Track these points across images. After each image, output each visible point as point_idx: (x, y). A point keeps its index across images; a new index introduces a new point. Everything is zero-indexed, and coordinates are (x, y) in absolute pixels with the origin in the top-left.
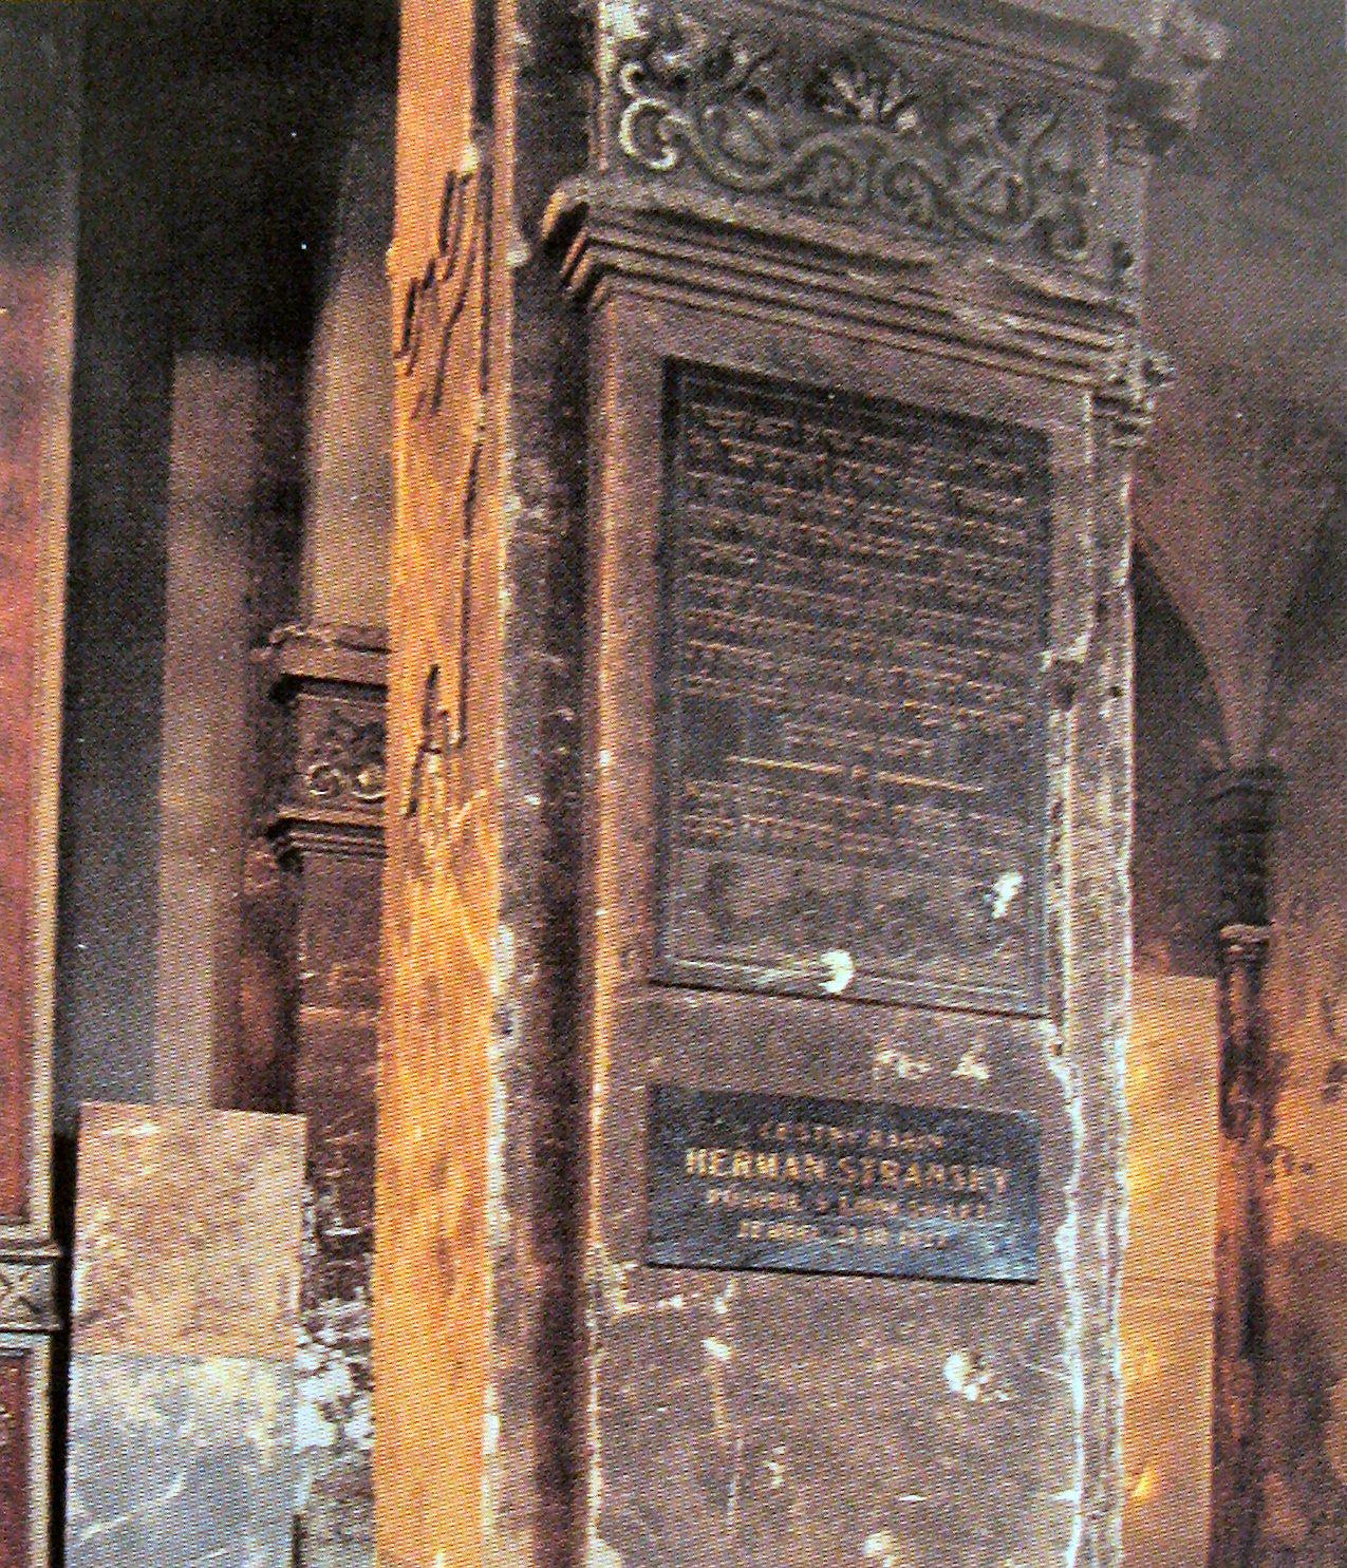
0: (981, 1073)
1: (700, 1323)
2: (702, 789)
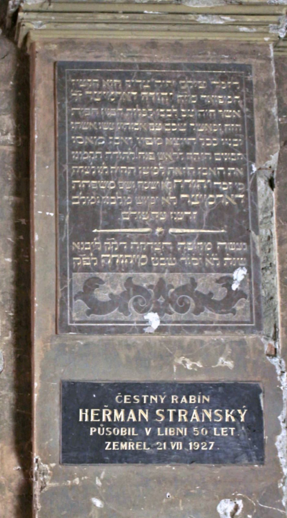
0: (230, 364)
1: (88, 490)
2: (81, 246)
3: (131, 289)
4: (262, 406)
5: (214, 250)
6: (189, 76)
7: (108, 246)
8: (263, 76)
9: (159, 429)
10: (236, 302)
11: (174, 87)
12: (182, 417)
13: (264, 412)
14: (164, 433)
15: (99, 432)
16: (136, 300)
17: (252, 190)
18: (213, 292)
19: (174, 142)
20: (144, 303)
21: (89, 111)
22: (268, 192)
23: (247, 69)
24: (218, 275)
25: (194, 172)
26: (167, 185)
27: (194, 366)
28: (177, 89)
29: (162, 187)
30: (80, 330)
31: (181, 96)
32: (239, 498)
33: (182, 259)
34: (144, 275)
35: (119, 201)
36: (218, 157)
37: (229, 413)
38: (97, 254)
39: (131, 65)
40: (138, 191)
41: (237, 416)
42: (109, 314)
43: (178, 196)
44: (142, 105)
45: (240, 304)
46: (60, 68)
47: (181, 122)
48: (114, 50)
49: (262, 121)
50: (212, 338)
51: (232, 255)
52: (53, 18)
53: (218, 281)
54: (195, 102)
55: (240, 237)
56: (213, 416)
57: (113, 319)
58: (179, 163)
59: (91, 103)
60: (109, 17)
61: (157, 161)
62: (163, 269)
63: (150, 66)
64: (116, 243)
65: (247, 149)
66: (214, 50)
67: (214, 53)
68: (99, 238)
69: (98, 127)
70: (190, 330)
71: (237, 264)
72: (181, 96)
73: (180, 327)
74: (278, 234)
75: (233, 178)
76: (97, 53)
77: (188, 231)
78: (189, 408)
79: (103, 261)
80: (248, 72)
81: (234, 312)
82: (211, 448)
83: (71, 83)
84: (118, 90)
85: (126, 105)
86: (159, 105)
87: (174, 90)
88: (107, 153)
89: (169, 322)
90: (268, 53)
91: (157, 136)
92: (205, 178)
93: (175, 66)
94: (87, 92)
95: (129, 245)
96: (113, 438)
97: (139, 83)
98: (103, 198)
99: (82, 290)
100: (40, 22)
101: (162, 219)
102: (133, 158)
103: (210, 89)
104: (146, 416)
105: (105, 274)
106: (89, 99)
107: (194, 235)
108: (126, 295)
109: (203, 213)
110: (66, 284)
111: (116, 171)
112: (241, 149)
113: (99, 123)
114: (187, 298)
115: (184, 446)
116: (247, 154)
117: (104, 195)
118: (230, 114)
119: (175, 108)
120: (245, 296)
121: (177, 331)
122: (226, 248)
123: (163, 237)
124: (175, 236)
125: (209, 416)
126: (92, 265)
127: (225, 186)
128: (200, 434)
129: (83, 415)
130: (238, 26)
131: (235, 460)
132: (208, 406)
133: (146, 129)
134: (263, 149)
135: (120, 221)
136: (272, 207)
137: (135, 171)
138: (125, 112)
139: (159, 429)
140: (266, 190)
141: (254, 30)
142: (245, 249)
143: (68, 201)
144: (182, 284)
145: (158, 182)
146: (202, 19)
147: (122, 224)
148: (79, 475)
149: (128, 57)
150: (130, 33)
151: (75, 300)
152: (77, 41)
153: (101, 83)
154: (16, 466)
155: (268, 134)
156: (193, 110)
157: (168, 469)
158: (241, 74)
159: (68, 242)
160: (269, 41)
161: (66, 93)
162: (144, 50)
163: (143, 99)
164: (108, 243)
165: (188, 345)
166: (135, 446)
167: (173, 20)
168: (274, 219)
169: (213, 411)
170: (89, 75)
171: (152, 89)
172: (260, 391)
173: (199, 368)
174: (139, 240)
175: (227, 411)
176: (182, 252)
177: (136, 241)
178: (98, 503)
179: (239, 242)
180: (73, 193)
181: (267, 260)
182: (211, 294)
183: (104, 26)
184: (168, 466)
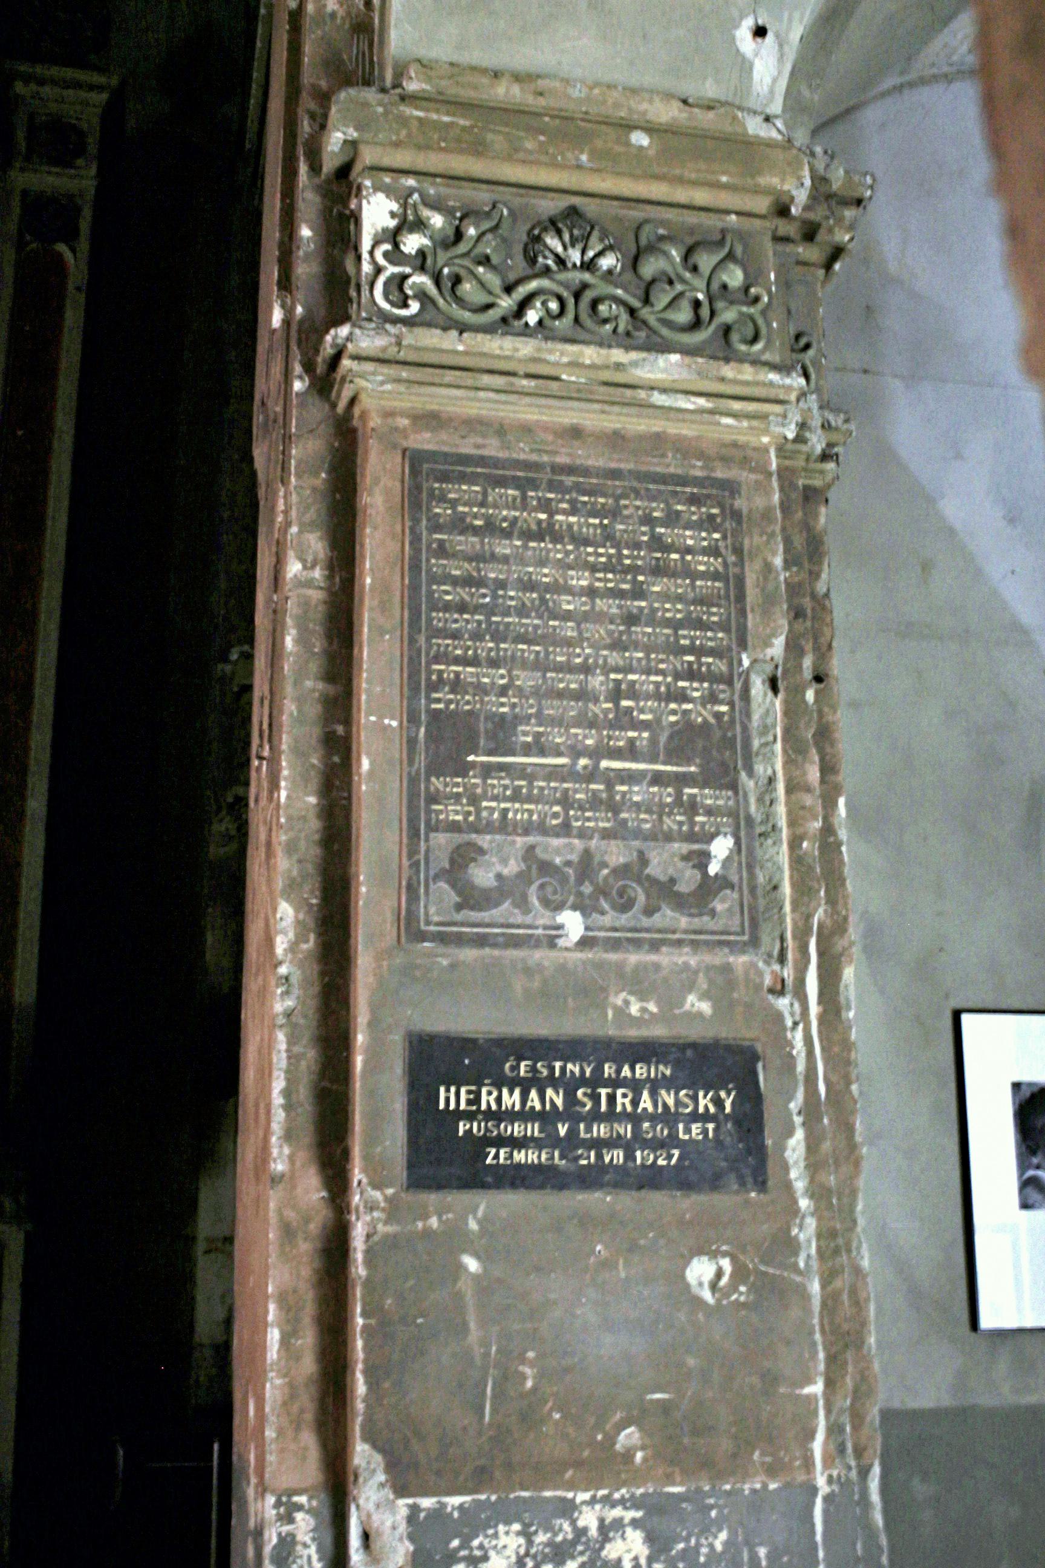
0: (705, 1007)
1: (454, 1240)
7: (494, 786)
9: (582, 1126)
10: (715, 896)
12: (488, 1102)
16: (542, 887)
20: (555, 892)
24: (685, 848)
25: (644, 663)
26: (597, 682)
27: (644, 1010)
28: (615, 513)
30: (442, 939)
32: (725, 1254)
33: (624, 815)
34: (556, 842)
35: (514, 706)
36: (685, 637)
37: (705, 1096)
38: (474, 800)
41: (719, 1103)
42: (494, 911)
45: (723, 901)
51: (709, 812)
53: (686, 858)
56: (678, 1103)
57: (502, 920)
58: (617, 645)
60: (499, 381)
62: (589, 832)
63: (570, 470)
64: (507, 782)
68: (478, 770)
70: (637, 944)
71: (717, 828)
75: (713, 678)
77: (634, 766)
78: (636, 1086)
79: (485, 814)
81: (713, 913)
83: (433, 490)
84: (515, 509)
88: (494, 619)
89: (600, 929)
93: (615, 474)
95: (530, 785)
98: (486, 699)
99: (447, 866)
103: (672, 519)
104: (559, 1102)
105: (488, 837)
107: (643, 774)
108: (524, 877)
112: (724, 626)
120: (732, 887)
121: (615, 945)
123: (591, 775)
124: (612, 774)
125: (671, 1101)
129: (449, 1098)
131: (715, 1183)
132: (670, 1083)
133: (561, 581)
136: (774, 726)
139: (582, 1126)
141: (745, 424)
143: (423, 701)
145: (582, 677)
146: (658, 398)
148: (437, 1212)
149: (532, 451)
153: (485, 494)
154: (318, 1191)
155: (769, 601)
157: (599, 1200)
159: (423, 776)
162: (560, 441)
164: (495, 782)
166: (539, 1157)
168: (778, 747)
169: (677, 1094)
171: (573, 511)
173: (651, 1014)
174: (548, 778)
175: (701, 1094)
176: (624, 803)
178: (472, 1264)
180: (433, 687)
182: (673, 881)
183: (492, 395)
184: (598, 1195)
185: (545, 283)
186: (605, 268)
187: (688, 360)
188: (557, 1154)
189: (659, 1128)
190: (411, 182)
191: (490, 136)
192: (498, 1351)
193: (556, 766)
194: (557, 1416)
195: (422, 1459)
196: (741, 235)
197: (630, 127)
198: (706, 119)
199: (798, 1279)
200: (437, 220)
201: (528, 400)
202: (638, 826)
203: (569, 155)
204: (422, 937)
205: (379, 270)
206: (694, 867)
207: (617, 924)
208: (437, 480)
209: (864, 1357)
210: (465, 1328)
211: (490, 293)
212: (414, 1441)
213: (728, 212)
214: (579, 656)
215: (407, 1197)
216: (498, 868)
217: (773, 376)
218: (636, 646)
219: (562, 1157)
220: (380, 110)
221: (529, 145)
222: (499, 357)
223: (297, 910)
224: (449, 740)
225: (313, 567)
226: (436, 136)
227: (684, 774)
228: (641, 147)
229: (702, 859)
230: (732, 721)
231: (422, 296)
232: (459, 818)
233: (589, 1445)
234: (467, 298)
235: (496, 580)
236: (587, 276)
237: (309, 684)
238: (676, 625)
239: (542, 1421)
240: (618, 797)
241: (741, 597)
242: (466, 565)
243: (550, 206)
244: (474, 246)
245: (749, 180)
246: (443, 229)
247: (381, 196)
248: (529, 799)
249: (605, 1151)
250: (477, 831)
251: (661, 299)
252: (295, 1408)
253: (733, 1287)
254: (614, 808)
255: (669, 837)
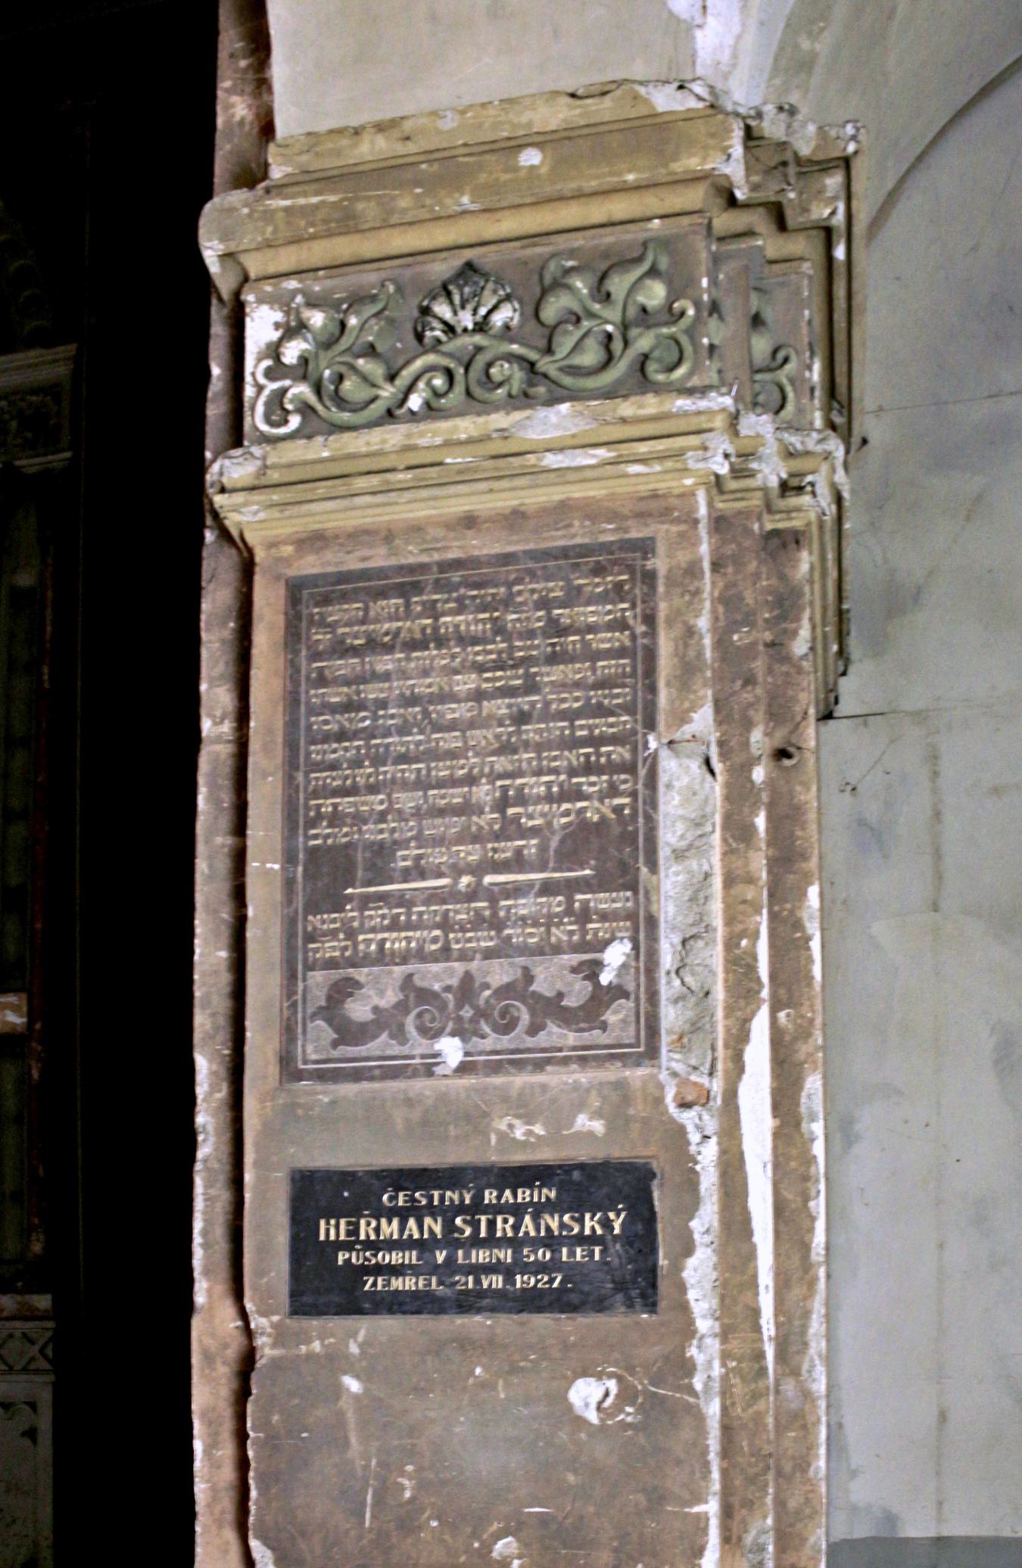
0: (598, 1126)
1: (335, 1362)
2: (323, 922)
3: (412, 996)
4: (656, 1203)
5: (569, 911)
6: (532, 574)
7: (371, 917)
8: (683, 558)
9: (460, 1253)
10: (608, 1007)
11: (501, 600)
12: (504, 1229)
13: (659, 1216)
14: (470, 1258)
15: (354, 1260)
16: (420, 1015)
17: (646, 785)
18: (564, 990)
19: (499, 708)
20: (433, 1020)
21: (344, 666)
22: (707, 785)
23: (645, 547)
24: (576, 958)
25: (534, 763)
26: (483, 792)
27: (529, 1133)
28: (508, 603)
29: (474, 801)
30: (321, 1076)
31: (514, 616)
32: (610, 1376)
33: (507, 932)
34: (435, 968)
35: (393, 831)
36: (582, 727)
37: (592, 1219)
38: (351, 934)
39: (423, 568)
40: (429, 809)
41: (607, 1224)
42: (370, 1045)
43: (503, 812)
44: (441, 642)
45: (615, 1012)
46: (295, 590)
47: (513, 667)
48: (397, 541)
49: (676, 649)
50: (564, 1078)
51: (604, 917)
52: (275, 497)
53: (574, 970)
54: (541, 624)
55: (621, 881)
56: (562, 1226)
57: (378, 1053)
58: (506, 748)
59: (347, 650)
60: (375, 481)
61: (467, 748)
62: (470, 953)
63: (457, 564)
64: (386, 911)
65: (640, 706)
66: (587, 517)
67: (587, 523)
68: (355, 903)
69: (358, 693)
70: (520, 1065)
71: (613, 934)
72: (514, 616)
73: (500, 1061)
74: (723, 867)
75: (612, 768)
76: (366, 552)
77: (521, 877)
78: (518, 1210)
79: (362, 947)
80: (646, 553)
81: (604, 1027)
82: (555, 1285)
83: (312, 615)
84: (398, 620)
85: (413, 645)
86: (474, 638)
87: (501, 608)
88: (374, 742)
89: (480, 1053)
90: (694, 509)
91: (467, 700)
92: (555, 771)
93: (507, 559)
94: (341, 631)
95: (409, 914)
96: (378, 1270)
97: (436, 601)
98: (365, 828)
99: (323, 1003)
100: (255, 507)
101: (471, 858)
102: (421, 748)
103: (574, 597)
104: (438, 1229)
105: (366, 970)
106: (342, 642)
107: (530, 884)
108: (402, 1007)
109: (549, 840)
110: (295, 993)
111: (389, 776)
112: (629, 709)
113: (362, 687)
114: (513, 1006)
115: (505, 1282)
116: (639, 717)
117: (365, 824)
118: (609, 640)
119: (502, 641)
120: (626, 995)
121: (496, 1068)
122: (592, 904)
123: (471, 896)
124: (496, 889)
125: (554, 1225)
126: (343, 954)
127: (593, 784)
128: (536, 1260)
129: (329, 1230)
130: (622, 466)
131: (600, 1305)
132: (550, 1207)
133: (446, 688)
134: (677, 703)
135: (394, 870)
136: (713, 814)
137: (424, 772)
138: (408, 659)
139: (460, 1253)
140: (703, 781)
141: (657, 468)
142: (629, 904)
143: (301, 839)
144: (506, 979)
145: (466, 789)
146: (551, 460)
147: (397, 874)
148: (322, 1336)
149: (423, 551)
150: (422, 505)
151: (312, 1021)
152: (328, 534)
153: (366, 610)
154: (234, 1320)
155: (688, 670)
156: (536, 642)
157: (478, 1323)
158: (634, 560)
159: (300, 917)
160: (696, 484)
161: (304, 637)
162: (452, 535)
163: (443, 631)
164: (372, 913)
165: (520, 1095)
166: (416, 1283)
167: (496, 469)
168: (716, 838)
169: (561, 1217)
170: (345, 597)
171: (461, 610)
172: (654, 1175)
173: (539, 1137)
174: (427, 902)
175: (588, 1216)
176: (508, 918)
177: (423, 905)
178: (353, 1385)
179: (617, 890)
180: (312, 823)
181: (701, 920)
182: (560, 995)
183: (368, 499)
184: (478, 1318)
185: (431, 358)
186: (499, 324)
187: (579, 406)
188: (434, 1280)
189: (540, 1252)
190: (292, 284)
191: (360, 206)
192: (379, 1464)
193: (436, 888)
194: (434, 1524)
195: (308, 1557)
196: (666, 243)
197: (516, 146)
198: (604, 109)
199: (691, 1400)
200: (317, 319)
201: (407, 496)
202: (524, 942)
203: (448, 201)
204: (299, 1075)
205: (260, 389)
206: (585, 978)
207: (499, 1047)
208: (317, 605)
209: (809, 1480)
210: (347, 1444)
211: (374, 385)
212: (300, 1540)
213: (649, 219)
214: (462, 768)
215: (294, 1323)
216: (376, 1001)
217: (683, 403)
218: (527, 745)
219: (440, 1283)
220: (246, 211)
221: (404, 203)
222: (367, 455)
223: (210, 1061)
224: (329, 876)
225: (221, 722)
226: (303, 223)
227: (577, 879)
228: (532, 167)
229: (592, 970)
230: (634, 810)
231: (305, 409)
232: (337, 954)
233: (465, 1552)
234: (349, 397)
235: (376, 700)
236: (478, 339)
237: (219, 840)
238: (571, 716)
239: (420, 1528)
240: (502, 914)
241: (650, 671)
242: (345, 689)
243: (442, 269)
244: (357, 337)
245: (663, 171)
246: (325, 325)
247: (265, 308)
248: (409, 926)
249: (483, 1277)
250: (354, 965)
251: (564, 344)
252: (217, 1509)
253: (618, 1408)
254: (497, 925)
255: (557, 950)
